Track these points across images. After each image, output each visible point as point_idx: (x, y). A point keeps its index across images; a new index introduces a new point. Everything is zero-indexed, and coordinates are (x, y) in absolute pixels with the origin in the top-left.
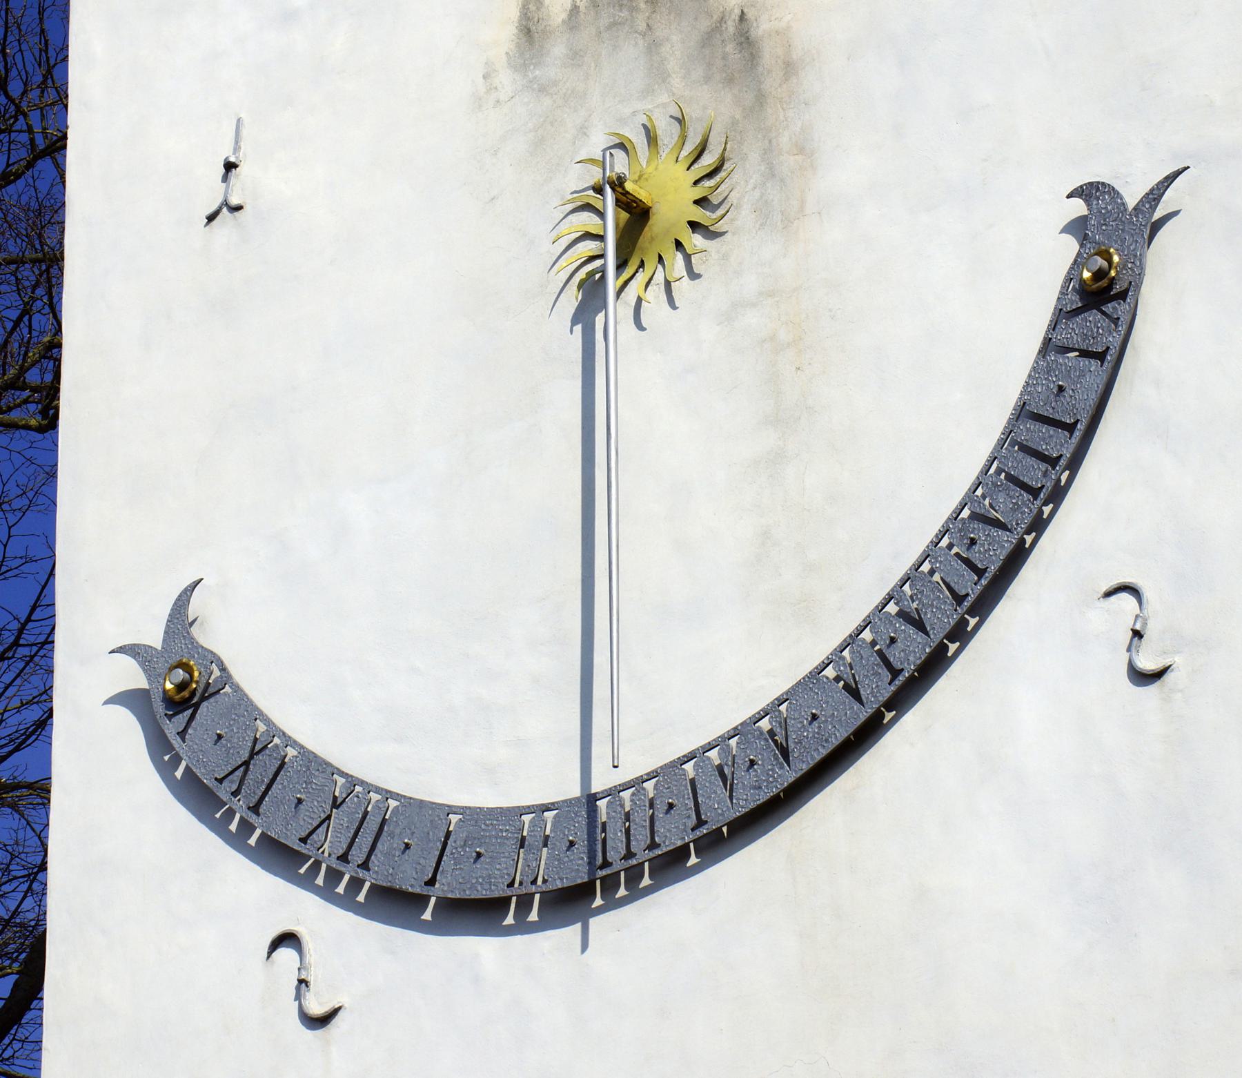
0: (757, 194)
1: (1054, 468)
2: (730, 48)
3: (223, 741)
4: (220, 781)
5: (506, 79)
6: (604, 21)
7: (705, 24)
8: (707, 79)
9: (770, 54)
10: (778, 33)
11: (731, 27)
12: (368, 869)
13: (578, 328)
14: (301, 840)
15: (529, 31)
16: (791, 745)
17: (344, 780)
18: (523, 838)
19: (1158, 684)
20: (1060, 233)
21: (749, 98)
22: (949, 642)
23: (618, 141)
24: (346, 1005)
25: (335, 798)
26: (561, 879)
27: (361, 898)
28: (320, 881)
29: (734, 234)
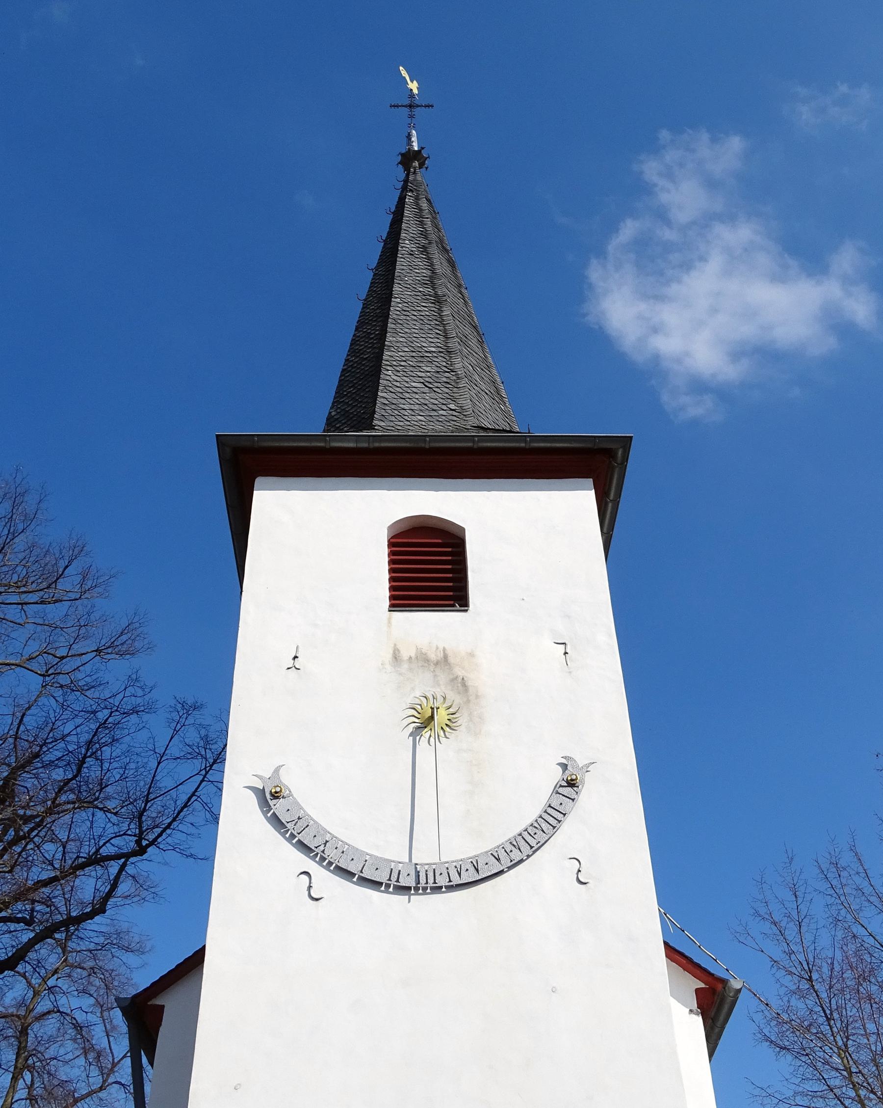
0: (466, 724)
1: (559, 823)
2: (459, 685)
3: (289, 812)
4: (288, 822)
5: (389, 668)
6: (420, 665)
7: (451, 677)
8: (452, 690)
9: (471, 690)
10: (474, 686)
11: (460, 680)
12: (556, 794)
13: (411, 738)
14: (315, 847)
15: (396, 658)
16: (479, 869)
17: (288, 792)
18: (727, 969)
19: (585, 885)
20: (557, 764)
21: (465, 699)
22: (142, 855)
23: (420, 703)
24: (325, 897)
25: (299, 817)
26: (405, 883)
27: (332, 868)
28: (317, 859)
29: (460, 731)
